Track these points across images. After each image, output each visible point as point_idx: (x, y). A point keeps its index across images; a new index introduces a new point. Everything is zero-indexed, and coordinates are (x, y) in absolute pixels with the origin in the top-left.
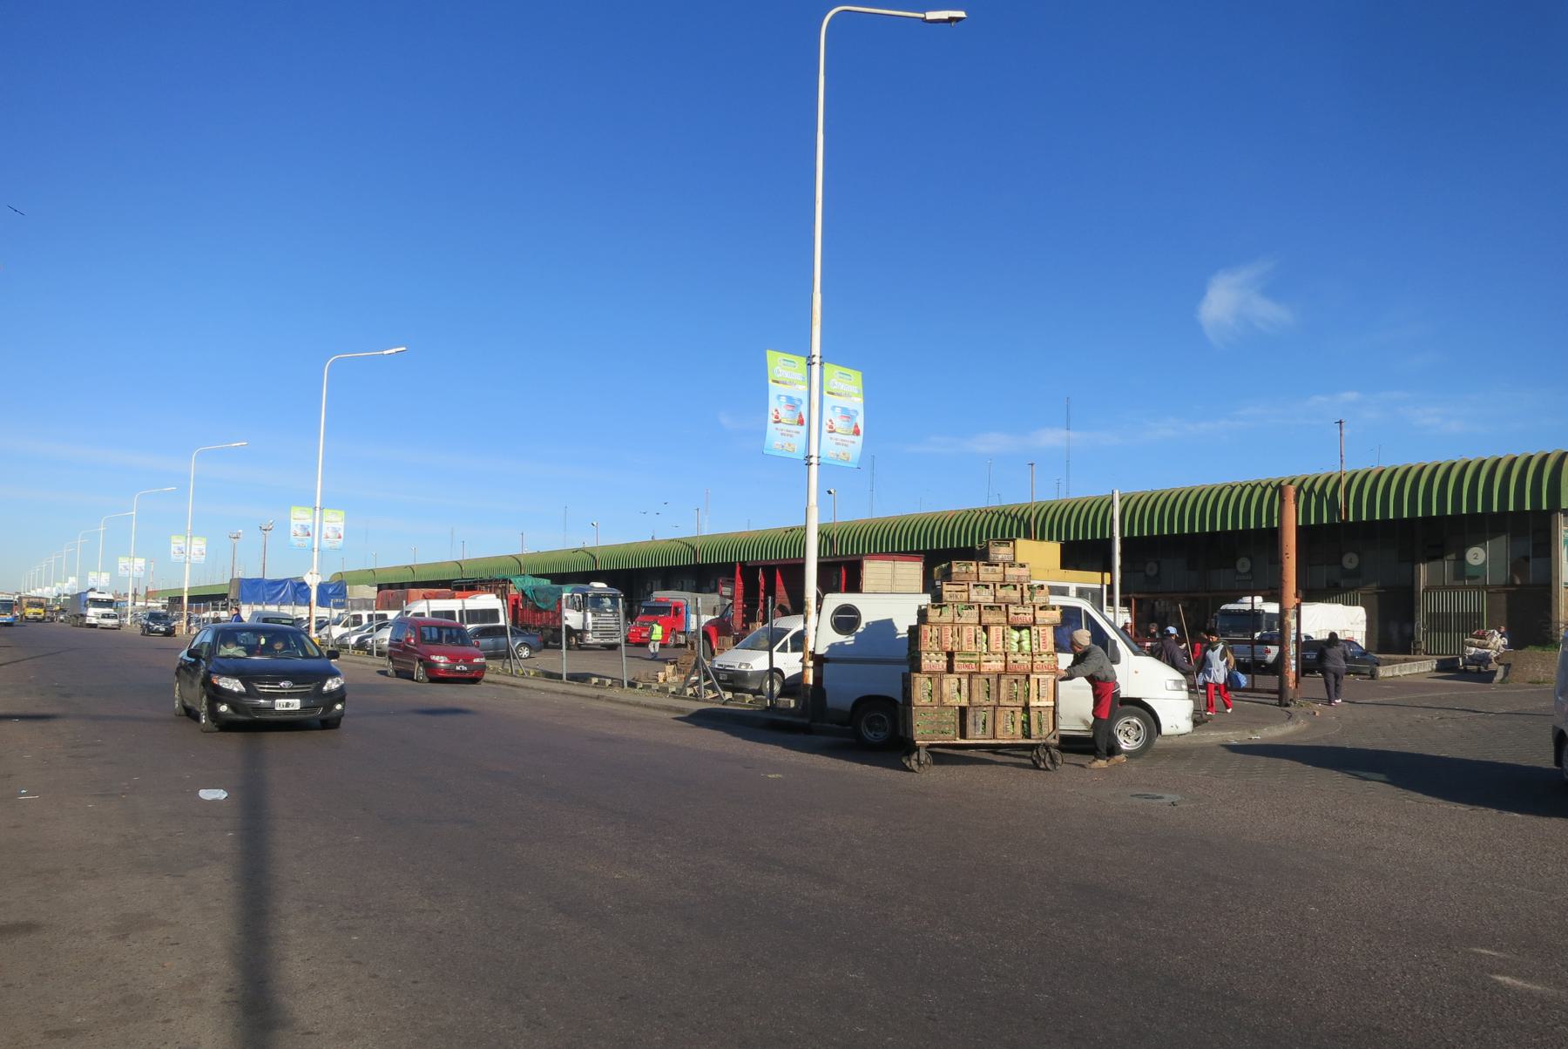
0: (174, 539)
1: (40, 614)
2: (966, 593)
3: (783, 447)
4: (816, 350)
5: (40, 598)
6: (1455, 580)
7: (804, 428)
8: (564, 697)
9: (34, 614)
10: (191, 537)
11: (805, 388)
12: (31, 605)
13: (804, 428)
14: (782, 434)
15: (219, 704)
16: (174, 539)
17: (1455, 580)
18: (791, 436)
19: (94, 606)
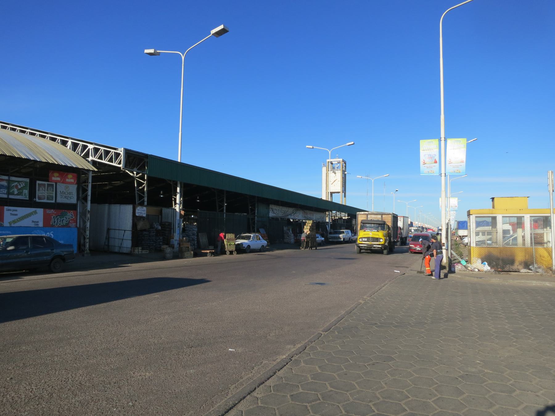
0: (424, 144)
1: (377, 240)
2: (25, 195)
3: (428, 172)
4: (443, 135)
5: (382, 214)
6: (496, 217)
7: (437, 165)
8: (525, 273)
9: (368, 239)
10: (445, 140)
11: (437, 150)
12: (180, 199)
13: (437, 165)
14: (427, 168)
15: (324, 240)
16: (424, 144)
17: (496, 217)
18: (432, 168)
19: (512, 235)
